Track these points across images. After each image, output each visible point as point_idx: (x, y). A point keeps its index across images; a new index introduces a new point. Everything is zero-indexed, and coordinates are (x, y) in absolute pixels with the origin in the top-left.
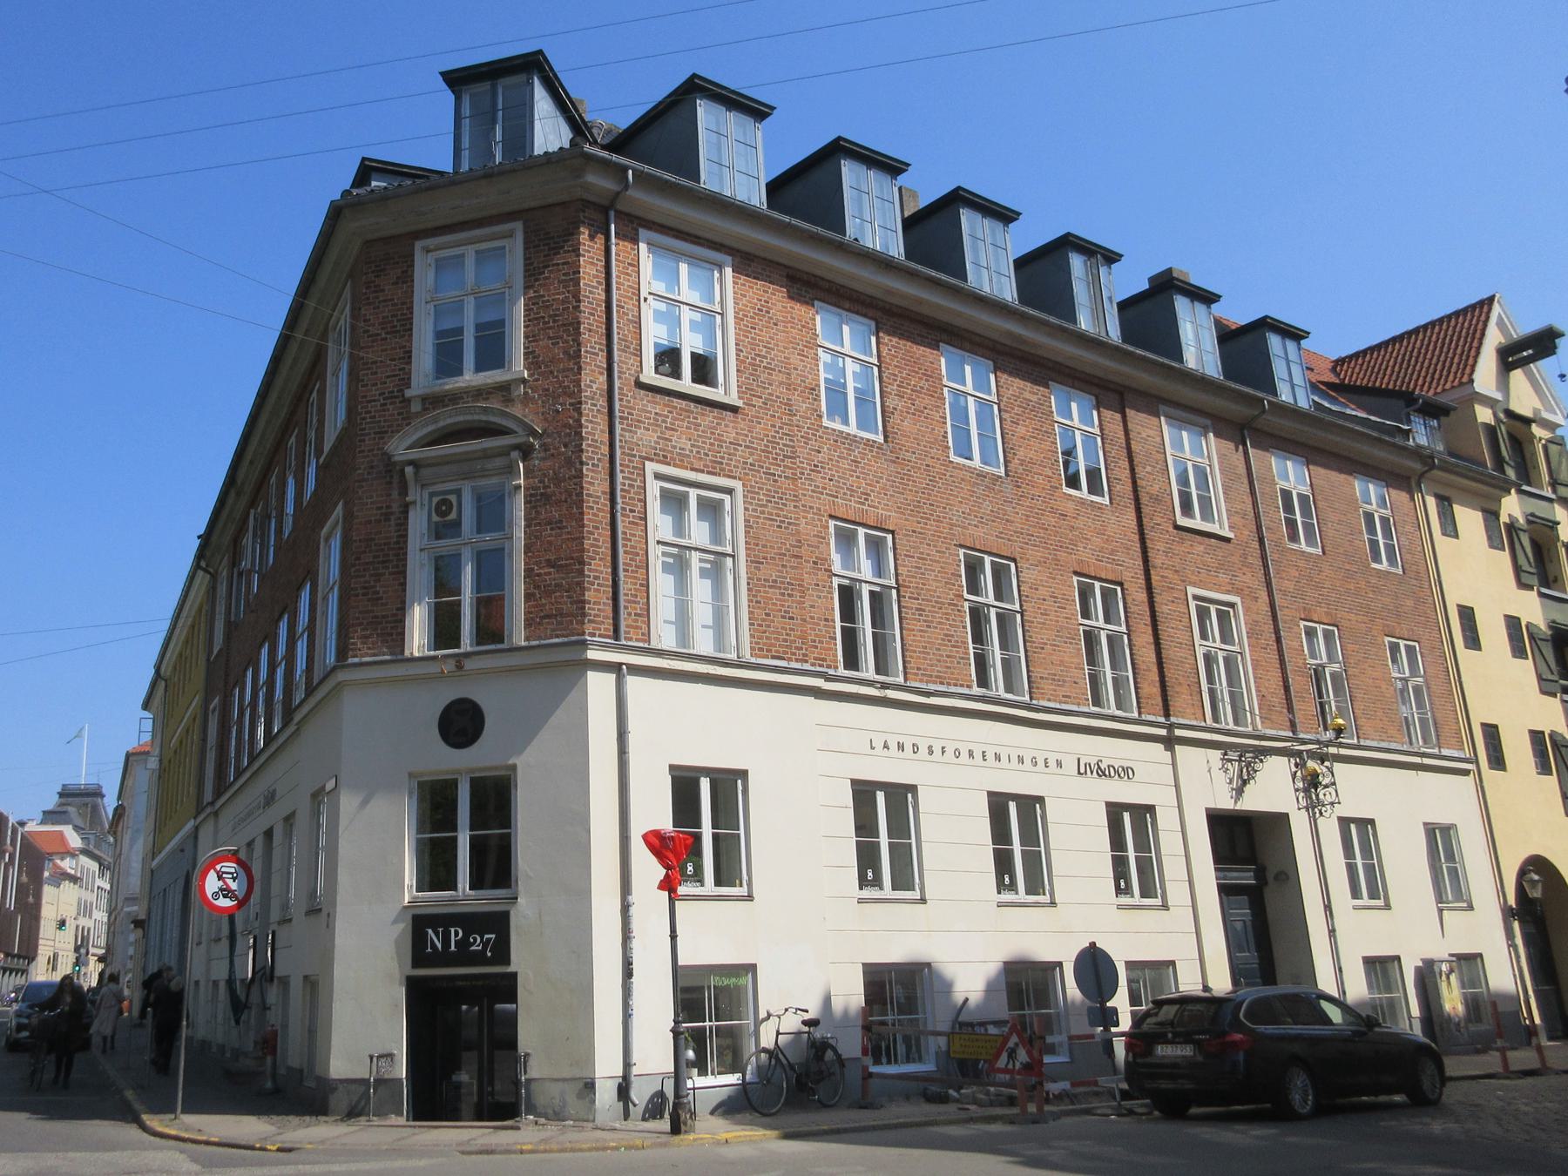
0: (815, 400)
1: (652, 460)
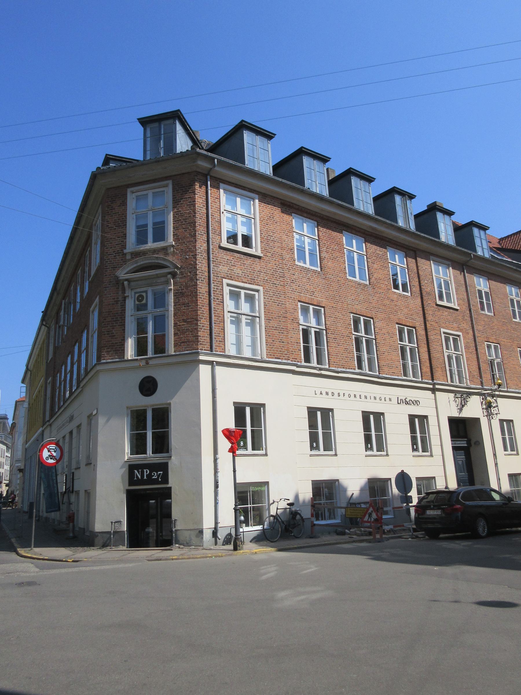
0: (293, 254)
1: (226, 278)
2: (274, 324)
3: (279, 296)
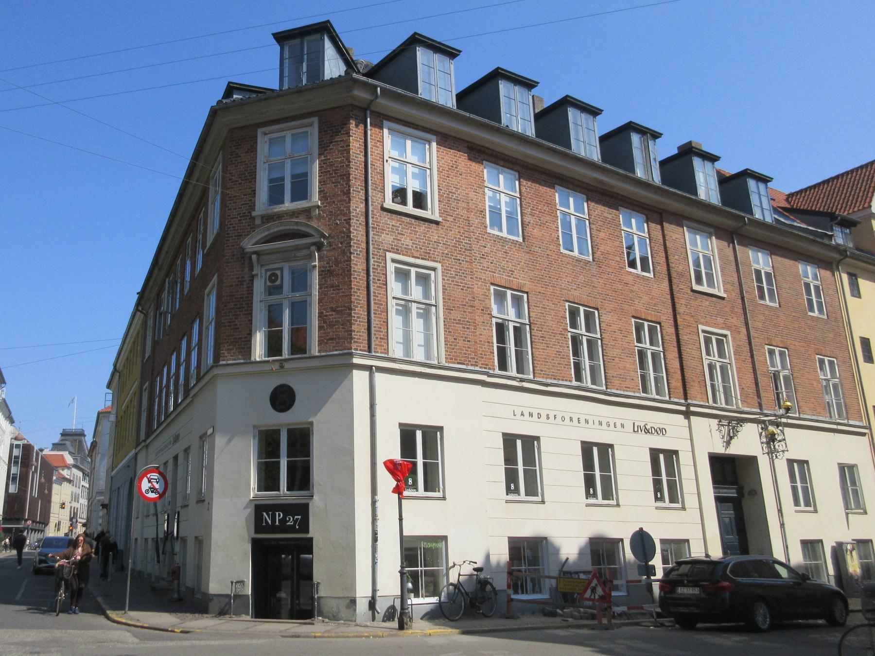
0: (483, 218)
1: (390, 251)
2: (456, 315)
3: (465, 277)
